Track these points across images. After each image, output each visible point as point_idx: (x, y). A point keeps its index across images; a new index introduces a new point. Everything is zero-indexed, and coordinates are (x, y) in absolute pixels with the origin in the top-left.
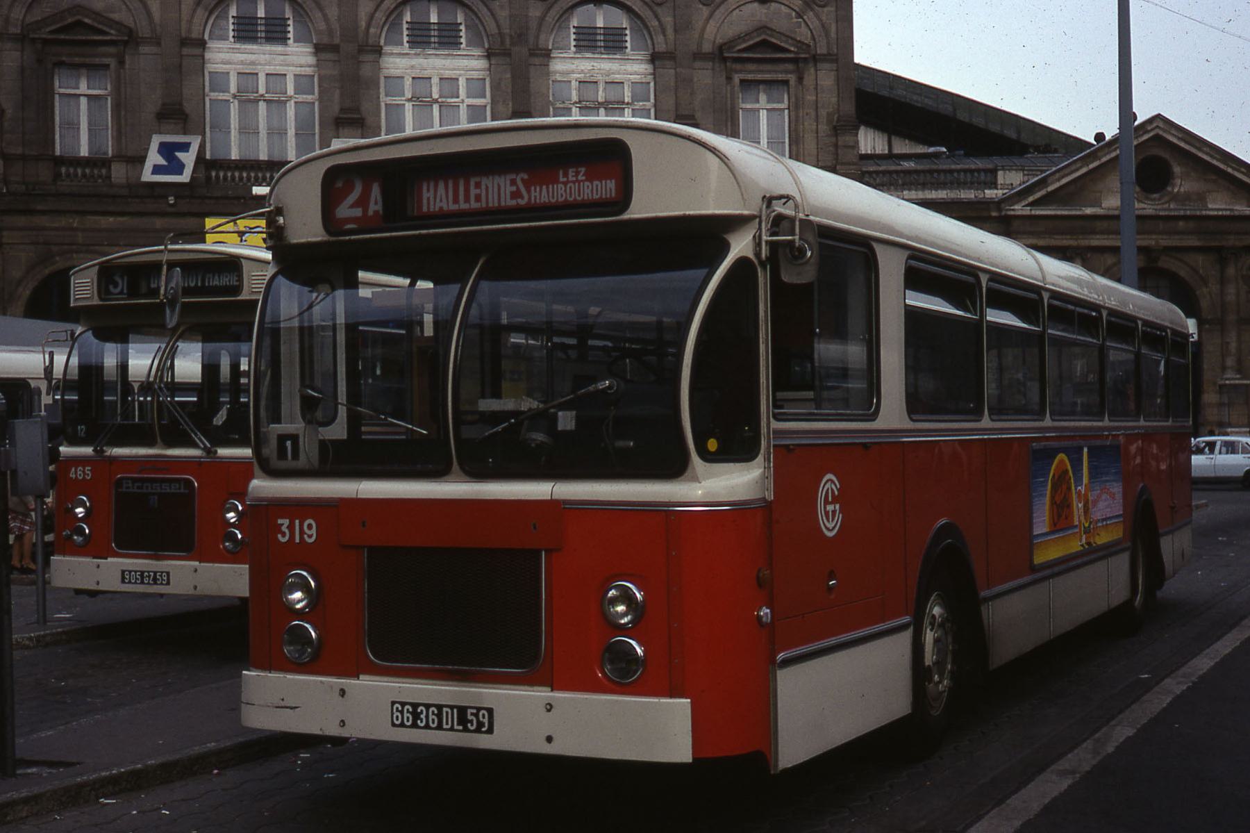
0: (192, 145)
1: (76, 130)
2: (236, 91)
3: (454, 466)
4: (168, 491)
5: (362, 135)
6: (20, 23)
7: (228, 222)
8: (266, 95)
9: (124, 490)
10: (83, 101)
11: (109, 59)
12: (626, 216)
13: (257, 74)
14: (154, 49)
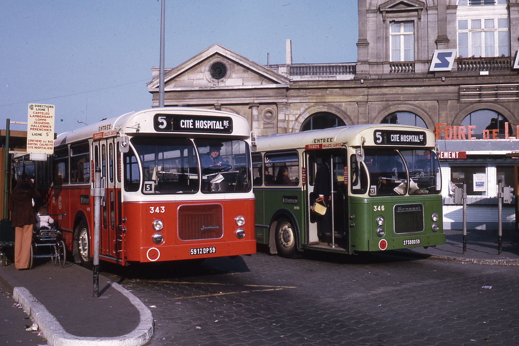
3: (359, 184)
6: (376, 5)
8: (485, 29)
9: (399, 211)
10: (402, 37)
11: (415, 18)
13: (480, 20)
14: (435, 12)
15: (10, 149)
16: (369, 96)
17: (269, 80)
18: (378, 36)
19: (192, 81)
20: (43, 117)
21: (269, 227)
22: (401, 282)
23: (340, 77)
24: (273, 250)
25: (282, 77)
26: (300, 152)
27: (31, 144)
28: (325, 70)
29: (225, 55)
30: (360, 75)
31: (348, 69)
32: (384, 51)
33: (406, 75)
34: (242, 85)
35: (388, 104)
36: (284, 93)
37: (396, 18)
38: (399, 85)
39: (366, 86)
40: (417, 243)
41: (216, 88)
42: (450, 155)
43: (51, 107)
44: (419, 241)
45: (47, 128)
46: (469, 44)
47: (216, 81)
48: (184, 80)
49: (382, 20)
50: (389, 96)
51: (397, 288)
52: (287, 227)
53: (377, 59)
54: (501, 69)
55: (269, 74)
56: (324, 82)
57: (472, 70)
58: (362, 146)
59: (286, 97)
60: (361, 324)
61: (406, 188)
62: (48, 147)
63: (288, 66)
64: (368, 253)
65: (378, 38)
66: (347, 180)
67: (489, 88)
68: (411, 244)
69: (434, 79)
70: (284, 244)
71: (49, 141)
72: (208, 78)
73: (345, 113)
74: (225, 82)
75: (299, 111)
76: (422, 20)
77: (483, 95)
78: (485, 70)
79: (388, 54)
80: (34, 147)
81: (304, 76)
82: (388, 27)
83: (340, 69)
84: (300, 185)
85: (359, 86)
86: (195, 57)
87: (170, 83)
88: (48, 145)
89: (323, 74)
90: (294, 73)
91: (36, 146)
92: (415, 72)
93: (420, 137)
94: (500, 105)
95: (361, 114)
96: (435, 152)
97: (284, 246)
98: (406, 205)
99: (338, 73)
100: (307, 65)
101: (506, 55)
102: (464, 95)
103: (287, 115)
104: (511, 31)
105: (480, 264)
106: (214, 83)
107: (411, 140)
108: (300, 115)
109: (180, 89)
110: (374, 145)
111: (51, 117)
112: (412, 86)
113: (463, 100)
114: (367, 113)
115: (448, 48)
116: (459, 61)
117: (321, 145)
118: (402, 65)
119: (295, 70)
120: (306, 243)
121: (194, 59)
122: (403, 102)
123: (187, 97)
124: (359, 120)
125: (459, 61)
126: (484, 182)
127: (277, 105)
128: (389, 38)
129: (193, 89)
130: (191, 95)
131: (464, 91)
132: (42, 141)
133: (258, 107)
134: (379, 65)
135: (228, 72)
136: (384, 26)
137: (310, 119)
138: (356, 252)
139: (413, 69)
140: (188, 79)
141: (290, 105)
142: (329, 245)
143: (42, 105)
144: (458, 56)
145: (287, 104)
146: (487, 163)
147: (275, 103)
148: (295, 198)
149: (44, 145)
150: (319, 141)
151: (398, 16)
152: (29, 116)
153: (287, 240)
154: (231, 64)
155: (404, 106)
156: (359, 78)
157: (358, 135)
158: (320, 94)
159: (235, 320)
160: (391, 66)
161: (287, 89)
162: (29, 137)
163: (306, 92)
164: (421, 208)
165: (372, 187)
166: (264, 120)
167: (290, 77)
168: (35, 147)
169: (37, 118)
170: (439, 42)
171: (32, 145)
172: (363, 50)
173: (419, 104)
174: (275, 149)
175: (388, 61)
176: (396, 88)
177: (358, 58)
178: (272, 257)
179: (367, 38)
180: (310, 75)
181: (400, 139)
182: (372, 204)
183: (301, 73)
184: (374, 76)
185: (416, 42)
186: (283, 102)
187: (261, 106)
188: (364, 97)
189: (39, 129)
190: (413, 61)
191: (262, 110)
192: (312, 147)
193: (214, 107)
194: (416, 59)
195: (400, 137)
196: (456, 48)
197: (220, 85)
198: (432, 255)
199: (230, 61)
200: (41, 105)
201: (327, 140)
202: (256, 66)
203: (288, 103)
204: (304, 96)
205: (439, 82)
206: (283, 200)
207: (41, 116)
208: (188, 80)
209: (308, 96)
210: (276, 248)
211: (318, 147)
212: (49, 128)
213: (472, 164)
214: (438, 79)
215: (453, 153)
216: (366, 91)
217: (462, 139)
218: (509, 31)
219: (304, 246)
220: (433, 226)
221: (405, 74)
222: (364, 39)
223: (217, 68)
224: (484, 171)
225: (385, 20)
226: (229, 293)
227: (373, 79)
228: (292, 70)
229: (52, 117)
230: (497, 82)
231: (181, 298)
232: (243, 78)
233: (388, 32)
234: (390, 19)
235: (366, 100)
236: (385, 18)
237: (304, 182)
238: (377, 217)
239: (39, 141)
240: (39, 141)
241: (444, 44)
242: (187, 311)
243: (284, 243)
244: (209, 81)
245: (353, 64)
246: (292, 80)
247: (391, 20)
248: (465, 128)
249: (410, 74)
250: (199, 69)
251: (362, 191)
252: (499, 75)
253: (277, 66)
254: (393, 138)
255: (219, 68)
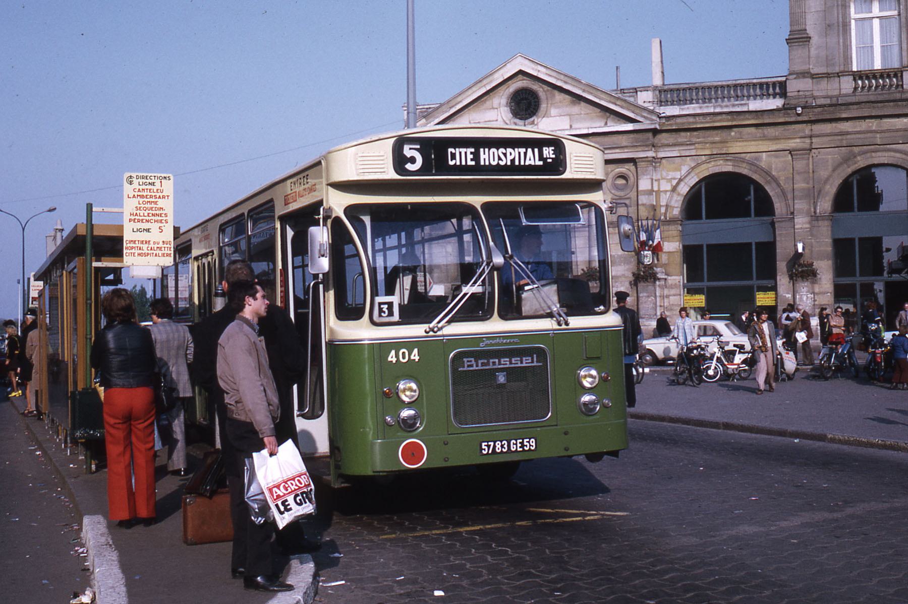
4: (519, 365)
5: (566, 227)
7: (454, 227)
9: (466, 369)
15: (93, 258)
16: (813, 139)
17: (619, 117)
18: (827, 22)
20: (151, 197)
23: (755, 105)
25: (645, 109)
27: (132, 248)
28: (726, 92)
29: (535, 74)
30: (795, 99)
32: (841, 51)
33: (885, 94)
34: (569, 128)
35: (851, 151)
43: (165, 178)
45: (160, 218)
51: (836, 515)
55: (619, 105)
56: (724, 116)
59: (653, 146)
60: (739, 594)
62: (163, 252)
63: (655, 88)
71: (163, 242)
72: (505, 119)
73: (768, 173)
74: (537, 124)
75: (679, 173)
79: (849, 57)
80: (136, 254)
82: (847, 4)
83: (755, 90)
86: (481, 81)
88: (163, 249)
89: (723, 101)
91: (141, 251)
92: (903, 88)
95: (799, 173)
99: (752, 97)
100: (691, 85)
103: (656, 180)
108: (680, 180)
111: (166, 197)
114: (811, 171)
118: (878, 76)
119: (669, 96)
121: (480, 85)
122: (882, 146)
124: (795, 186)
128: (850, 25)
132: (151, 243)
134: (832, 78)
135: (543, 106)
137: (700, 189)
139: (901, 83)
141: (660, 162)
143: (150, 175)
145: (655, 162)
147: (632, 161)
149: (155, 249)
152: (171, 197)
154: (548, 90)
155: (886, 154)
156: (792, 105)
158: (717, 139)
159: (485, 583)
160: (855, 80)
161: (655, 132)
162: (128, 236)
166: (613, 192)
167: (659, 109)
168: (139, 254)
169: (141, 200)
171: (133, 251)
172: (799, 52)
177: (790, 67)
179: (807, 29)
180: (698, 103)
184: (822, 99)
186: (647, 157)
188: (803, 140)
189: (144, 221)
200: (147, 174)
202: (594, 91)
203: (658, 158)
204: (687, 145)
207: (149, 197)
209: (694, 144)
212: (165, 218)
216: (807, 129)
222: (801, 30)
223: (522, 99)
226: (489, 526)
227: (820, 106)
228: (663, 96)
229: (168, 196)
231: (394, 536)
232: (569, 115)
235: (807, 146)
239: (146, 243)
240: (146, 243)
242: (393, 565)
245: (779, 79)
250: (488, 104)
253: (635, 91)
255: (526, 99)
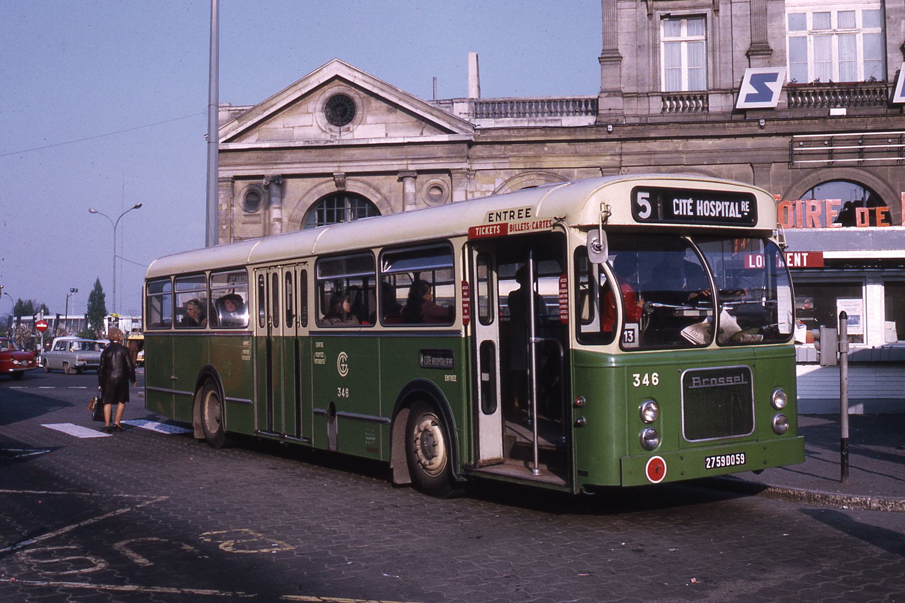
0: (779, 75)
1: (678, 71)
2: (812, 29)
3: (595, 319)
4: (732, 384)
8: (838, 30)
9: (694, 386)
10: (684, 46)
11: (707, 9)
12: (755, 228)
13: (830, 12)
16: (623, 156)
19: (292, 129)
21: (390, 421)
22: (704, 579)
23: (568, 121)
24: (401, 476)
25: (461, 120)
26: (458, 244)
28: (540, 107)
29: (352, 81)
31: (583, 106)
33: (692, 115)
36: (463, 151)
37: (671, 9)
38: (680, 135)
39: (617, 137)
40: (738, 463)
41: (336, 143)
42: (790, 260)
44: (743, 459)
46: (809, 59)
47: (336, 129)
48: (275, 128)
49: (646, 14)
50: (660, 156)
52: (429, 422)
53: (637, 86)
54: (869, 105)
55: (435, 115)
56: (538, 131)
57: (815, 107)
58: (602, 225)
59: (468, 158)
61: (713, 331)
64: (619, 489)
65: (639, 47)
66: (567, 309)
67: (848, 140)
68: (723, 465)
69: (745, 124)
70: (423, 462)
74: (352, 132)
76: (721, 13)
77: (837, 153)
78: (839, 106)
79: (658, 78)
81: (501, 119)
82: (657, 27)
84: (458, 325)
85: (604, 137)
87: (249, 133)
89: (537, 116)
90: (483, 114)
92: (708, 110)
93: (743, 206)
94: (868, 171)
96: (777, 243)
97: (424, 466)
98: (715, 370)
99: (565, 113)
101: (879, 79)
102: (800, 154)
103: (470, 192)
104: (887, 32)
105: (887, 510)
106: (333, 134)
107: (720, 212)
109: (267, 145)
110: (631, 224)
112: (704, 137)
113: (799, 162)
115: (770, 64)
116: (792, 89)
117: (504, 227)
118: (685, 98)
119: (484, 108)
120: (472, 463)
121: (295, 88)
123: (282, 160)
125: (792, 89)
126: (859, 316)
127: (450, 175)
128: (660, 47)
129: (292, 146)
130: (289, 156)
131: (801, 146)
133: (416, 178)
134: (642, 98)
135: (359, 113)
136: (650, 25)
138: (589, 487)
139: (706, 106)
140: (284, 125)
142: (527, 466)
144: (789, 81)
145: (469, 174)
146: (865, 277)
148: (447, 354)
150: (500, 217)
151: (677, 6)
153: (430, 453)
154: (364, 97)
156: (605, 122)
157: (593, 198)
158: (531, 153)
160: (663, 100)
161: (470, 144)
163: (505, 150)
164: (748, 378)
165: (628, 326)
166: (427, 202)
167: (475, 121)
170: (752, 55)
172: (611, 71)
173: (717, 170)
174: (403, 240)
175: (659, 91)
176: (675, 141)
178: (398, 492)
179: (619, 48)
181: (694, 209)
182: (628, 369)
183: (495, 113)
184: (632, 118)
185: (710, 54)
186: (461, 169)
187: (421, 176)
190: (705, 89)
191: (422, 185)
192: (484, 231)
193: (333, 178)
194: (711, 86)
195: (694, 206)
196: (785, 65)
197: (343, 138)
198: (770, 487)
199: (362, 93)
201: (519, 214)
203: (473, 171)
204: (502, 158)
205: (755, 129)
206: (419, 360)
208: (284, 127)
209: (508, 157)
210: (407, 470)
211: (496, 230)
213: (835, 278)
214: (752, 124)
215: (796, 254)
216: (617, 146)
217: (814, 226)
218: (883, 33)
219: (467, 468)
220: (775, 421)
221: (691, 113)
223: (338, 105)
224: (858, 295)
225: (652, 14)
227: (630, 125)
230: (863, 128)
233: (658, 35)
234: (661, 12)
235: (617, 164)
236: (651, 9)
237: (466, 317)
238: (641, 403)
241: (763, 58)
243: (424, 460)
244: (324, 129)
246: (478, 127)
247: (663, 13)
248: (820, 206)
249: (698, 115)
250: (304, 107)
251: (605, 337)
252: (865, 116)
253: (451, 101)
254: (678, 208)
255: (342, 105)
